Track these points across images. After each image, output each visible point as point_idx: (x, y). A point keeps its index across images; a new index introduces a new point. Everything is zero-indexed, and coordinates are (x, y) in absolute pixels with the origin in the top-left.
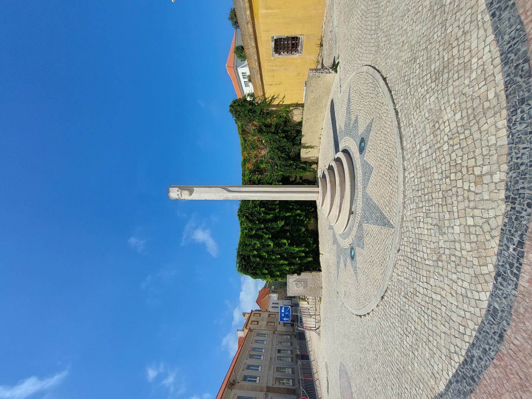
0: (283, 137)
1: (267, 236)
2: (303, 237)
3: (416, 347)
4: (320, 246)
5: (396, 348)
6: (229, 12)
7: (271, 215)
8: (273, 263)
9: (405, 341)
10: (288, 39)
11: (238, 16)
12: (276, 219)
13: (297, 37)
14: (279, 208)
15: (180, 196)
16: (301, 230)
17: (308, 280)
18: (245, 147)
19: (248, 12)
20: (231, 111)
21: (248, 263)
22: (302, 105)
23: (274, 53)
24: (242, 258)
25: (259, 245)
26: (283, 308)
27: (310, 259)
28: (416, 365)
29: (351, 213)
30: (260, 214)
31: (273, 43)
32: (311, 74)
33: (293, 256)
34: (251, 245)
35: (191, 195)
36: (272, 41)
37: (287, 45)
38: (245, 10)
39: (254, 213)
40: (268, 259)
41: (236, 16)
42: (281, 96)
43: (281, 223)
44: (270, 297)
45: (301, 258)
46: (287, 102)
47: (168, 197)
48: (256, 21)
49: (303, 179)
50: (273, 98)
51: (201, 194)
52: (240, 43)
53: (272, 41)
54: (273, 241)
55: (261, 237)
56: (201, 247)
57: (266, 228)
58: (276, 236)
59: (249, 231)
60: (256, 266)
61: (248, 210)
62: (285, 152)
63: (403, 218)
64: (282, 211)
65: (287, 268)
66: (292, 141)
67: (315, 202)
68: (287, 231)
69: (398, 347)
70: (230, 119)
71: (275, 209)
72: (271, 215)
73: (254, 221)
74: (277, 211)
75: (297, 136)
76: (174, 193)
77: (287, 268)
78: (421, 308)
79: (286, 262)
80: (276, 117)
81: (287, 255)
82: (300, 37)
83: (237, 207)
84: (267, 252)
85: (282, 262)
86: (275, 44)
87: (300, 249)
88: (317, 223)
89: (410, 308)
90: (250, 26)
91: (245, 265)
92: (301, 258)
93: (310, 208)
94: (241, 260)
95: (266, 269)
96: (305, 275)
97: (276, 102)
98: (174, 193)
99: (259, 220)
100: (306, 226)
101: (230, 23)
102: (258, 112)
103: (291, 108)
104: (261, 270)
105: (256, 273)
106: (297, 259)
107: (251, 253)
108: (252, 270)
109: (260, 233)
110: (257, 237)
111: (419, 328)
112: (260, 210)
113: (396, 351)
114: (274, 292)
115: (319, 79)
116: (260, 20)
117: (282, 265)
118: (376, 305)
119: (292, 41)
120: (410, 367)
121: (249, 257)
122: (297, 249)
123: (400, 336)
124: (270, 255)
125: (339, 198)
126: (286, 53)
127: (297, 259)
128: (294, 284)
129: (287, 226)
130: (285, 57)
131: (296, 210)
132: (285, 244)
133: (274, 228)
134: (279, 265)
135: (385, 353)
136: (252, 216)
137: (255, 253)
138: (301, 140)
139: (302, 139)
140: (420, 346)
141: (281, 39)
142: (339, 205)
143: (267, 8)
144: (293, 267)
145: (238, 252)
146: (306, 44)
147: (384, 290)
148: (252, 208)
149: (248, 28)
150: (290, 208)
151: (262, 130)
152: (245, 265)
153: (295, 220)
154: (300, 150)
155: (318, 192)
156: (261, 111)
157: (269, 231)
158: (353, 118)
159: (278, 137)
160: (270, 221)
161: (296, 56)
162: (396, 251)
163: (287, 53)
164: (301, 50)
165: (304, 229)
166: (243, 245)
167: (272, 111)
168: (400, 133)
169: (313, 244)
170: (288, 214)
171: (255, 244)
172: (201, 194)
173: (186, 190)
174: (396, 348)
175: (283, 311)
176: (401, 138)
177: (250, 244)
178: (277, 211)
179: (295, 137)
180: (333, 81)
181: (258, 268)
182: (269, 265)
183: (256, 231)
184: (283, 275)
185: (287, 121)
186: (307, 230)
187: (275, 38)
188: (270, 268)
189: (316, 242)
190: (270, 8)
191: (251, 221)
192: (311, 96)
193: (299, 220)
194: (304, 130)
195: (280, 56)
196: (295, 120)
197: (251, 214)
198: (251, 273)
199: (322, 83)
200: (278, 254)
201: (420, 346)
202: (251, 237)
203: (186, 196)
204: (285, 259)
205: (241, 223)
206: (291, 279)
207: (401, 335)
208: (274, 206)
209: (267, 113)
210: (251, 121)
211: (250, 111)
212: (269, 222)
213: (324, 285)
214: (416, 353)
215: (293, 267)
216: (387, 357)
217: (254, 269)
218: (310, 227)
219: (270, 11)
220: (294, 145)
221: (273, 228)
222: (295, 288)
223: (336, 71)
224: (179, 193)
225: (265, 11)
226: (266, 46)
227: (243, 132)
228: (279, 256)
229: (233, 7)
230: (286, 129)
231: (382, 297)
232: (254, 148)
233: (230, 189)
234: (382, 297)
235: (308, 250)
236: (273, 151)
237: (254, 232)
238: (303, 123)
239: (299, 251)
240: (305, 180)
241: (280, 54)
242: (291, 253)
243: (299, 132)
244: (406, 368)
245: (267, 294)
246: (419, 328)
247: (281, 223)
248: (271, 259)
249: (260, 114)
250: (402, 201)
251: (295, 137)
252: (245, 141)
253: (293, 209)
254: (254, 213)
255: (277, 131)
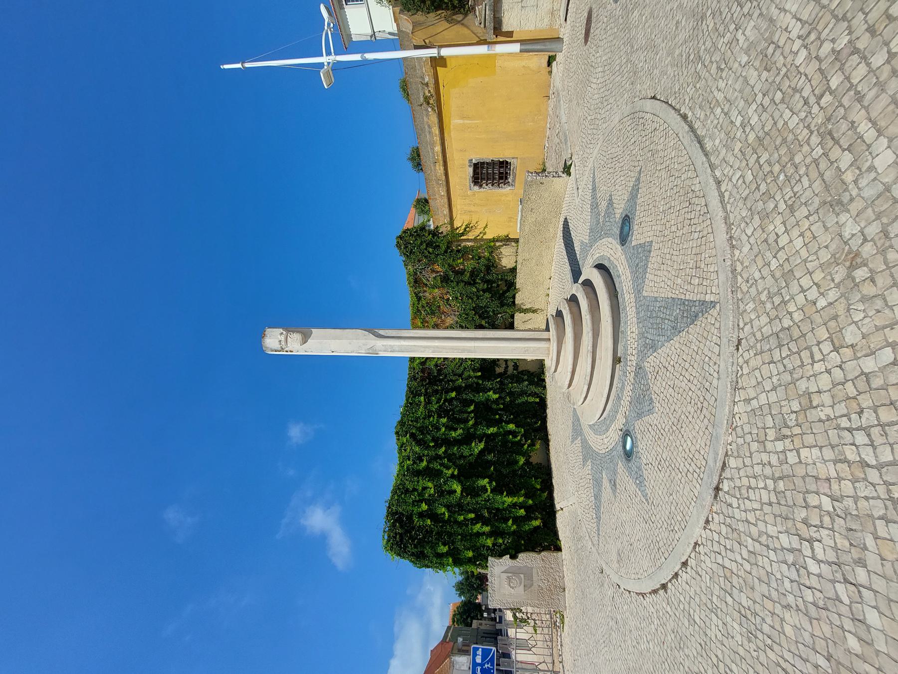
0: (484, 291)
1: (450, 472)
2: (521, 476)
3: (855, 553)
4: (555, 495)
5: (788, 607)
6: (409, 151)
7: (460, 431)
8: (460, 531)
9: (810, 562)
10: (493, 163)
11: (421, 154)
12: (467, 439)
13: (507, 162)
14: (476, 417)
15: (283, 343)
16: (517, 462)
17: (534, 571)
18: (418, 311)
19: (438, 148)
20: (398, 246)
21: (407, 531)
22: (517, 241)
23: (472, 185)
24: (396, 521)
25: (432, 491)
26: (479, 652)
27: (537, 523)
28: (872, 617)
29: (617, 360)
30: (439, 429)
31: (471, 170)
32: (529, 179)
33: (499, 515)
34: (415, 490)
35: (304, 341)
36: (470, 166)
37: (490, 173)
38: (433, 144)
39: (427, 427)
40: (448, 521)
41: (419, 155)
42: (481, 225)
43: (478, 447)
44: (452, 664)
45: (516, 520)
46: (489, 236)
47: (261, 346)
48: (446, 135)
49: (520, 369)
50: (468, 228)
51: (326, 343)
52: (424, 195)
53: (470, 166)
54: (460, 481)
55: (439, 474)
56: (321, 540)
57: (450, 457)
58: (469, 472)
59: (414, 463)
60: (424, 537)
61: (417, 421)
62: (488, 317)
63: (734, 271)
64: (481, 424)
65: (489, 542)
66: (499, 298)
67: (541, 364)
68: (490, 463)
69: (790, 599)
70: (397, 258)
71: (467, 421)
72: (460, 431)
73: (425, 443)
74: (471, 423)
75: (508, 290)
76: (274, 340)
77: (489, 542)
78: (838, 427)
79: (487, 529)
80: (472, 259)
81: (490, 513)
82: (512, 161)
83: (395, 399)
84: (448, 507)
85: (477, 527)
86: (474, 171)
87: (515, 499)
88: (549, 450)
89: (804, 453)
90: (440, 169)
91: (401, 535)
92: (516, 520)
93: (534, 375)
94: (394, 525)
95: (444, 545)
96: (526, 559)
97: (471, 236)
98: (274, 340)
99: (434, 439)
100: (526, 454)
101: (410, 165)
102: (444, 248)
103: (498, 244)
104: (434, 547)
105: (422, 553)
106: (510, 522)
107: (415, 509)
108: (416, 547)
109: (436, 466)
110: (431, 474)
111: (847, 487)
112: (438, 421)
113: (787, 615)
114: (463, 652)
115: (543, 187)
116: (453, 134)
117: (478, 534)
118: (702, 522)
119: (500, 167)
120: (853, 643)
121: (410, 517)
122: (509, 500)
123: (790, 558)
124: (455, 512)
125: (590, 334)
126: (490, 185)
127: (510, 522)
128: (505, 581)
129: (489, 453)
130: (488, 192)
131: (508, 423)
132: (484, 489)
133: (465, 457)
134: (471, 535)
135: (753, 646)
136: (422, 433)
137: (424, 507)
138: (514, 297)
139: (517, 295)
140: (870, 542)
141: (483, 163)
142: (590, 348)
143: (463, 118)
144: (501, 541)
145: (389, 507)
146: (519, 173)
147: (719, 464)
148: (424, 419)
149: (435, 170)
150: (496, 420)
151: (449, 279)
152: (401, 535)
153: (505, 442)
154: (512, 317)
155: (549, 340)
156: (448, 247)
157: (454, 464)
158: (603, 205)
159: (474, 290)
160: (458, 442)
161: (506, 190)
162: (732, 349)
163: (493, 185)
164: (514, 181)
165: (522, 460)
166: (401, 491)
167: (465, 247)
168: (697, 136)
169: (542, 490)
170: (492, 430)
171: (424, 489)
172: (326, 343)
173: (298, 332)
174: (788, 607)
175: (479, 660)
176: (699, 142)
177: (415, 490)
178: (471, 423)
179: (505, 292)
180: (565, 191)
181: (428, 542)
182: (450, 535)
183: (429, 462)
184: (480, 558)
185: (491, 265)
186: (527, 463)
187: (474, 161)
188: (453, 543)
189: (548, 486)
190: (468, 118)
191: (419, 443)
192: (531, 218)
193: (513, 443)
194: (519, 282)
195: (482, 190)
196: (504, 264)
197: (422, 430)
198: (413, 554)
199: (546, 195)
200: (470, 511)
201: (870, 542)
202: (418, 473)
203: (295, 345)
204: (485, 522)
205: (402, 446)
206: (498, 569)
207: (791, 550)
208: (465, 415)
209: (458, 251)
210: (432, 262)
211: (429, 244)
212: (454, 446)
213: (568, 584)
214: (861, 575)
215: (501, 541)
216: (763, 658)
217: (419, 543)
218: (535, 459)
219: (466, 122)
220: (502, 305)
221: (462, 457)
222: (506, 589)
223: (569, 174)
224: (282, 338)
225: (461, 121)
226: (461, 175)
227: (416, 282)
228: (472, 516)
229: (415, 145)
230: (489, 277)
231: (717, 489)
232: (433, 313)
233: (382, 332)
234: (717, 489)
235: (530, 502)
236: (467, 314)
237: (424, 463)
238: (519, 267)
239: (514, 505)
240: (522, 372)
241: (481, 186)
242: (498, 509)
243: (511, 285)
244: (839, 654)
245: (448, 656)
246: (847, 487)
247: (478, 447)
248: (456, 522)
249: (446, 252)
250: (725, 237)
251: (505, 292)
252: (419, 299)
253: (500, 421)
254: (427, 427)
255: (474, 280)
